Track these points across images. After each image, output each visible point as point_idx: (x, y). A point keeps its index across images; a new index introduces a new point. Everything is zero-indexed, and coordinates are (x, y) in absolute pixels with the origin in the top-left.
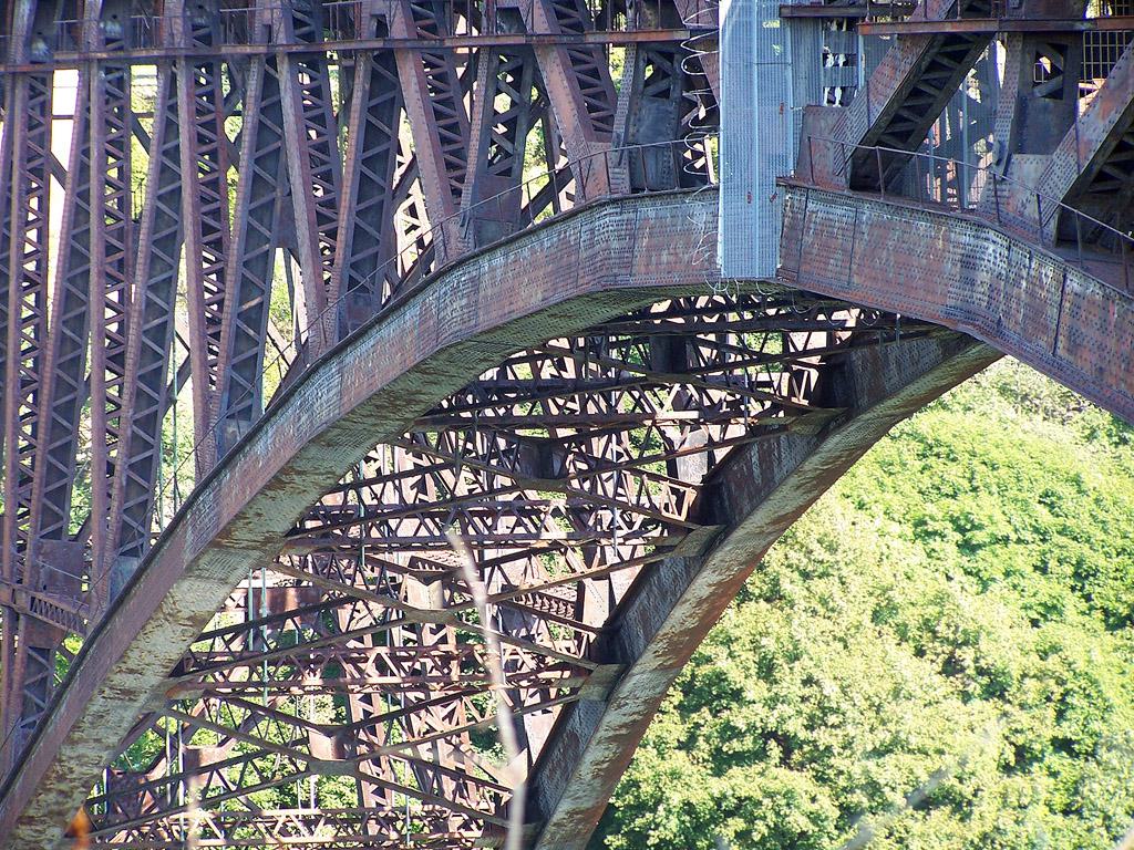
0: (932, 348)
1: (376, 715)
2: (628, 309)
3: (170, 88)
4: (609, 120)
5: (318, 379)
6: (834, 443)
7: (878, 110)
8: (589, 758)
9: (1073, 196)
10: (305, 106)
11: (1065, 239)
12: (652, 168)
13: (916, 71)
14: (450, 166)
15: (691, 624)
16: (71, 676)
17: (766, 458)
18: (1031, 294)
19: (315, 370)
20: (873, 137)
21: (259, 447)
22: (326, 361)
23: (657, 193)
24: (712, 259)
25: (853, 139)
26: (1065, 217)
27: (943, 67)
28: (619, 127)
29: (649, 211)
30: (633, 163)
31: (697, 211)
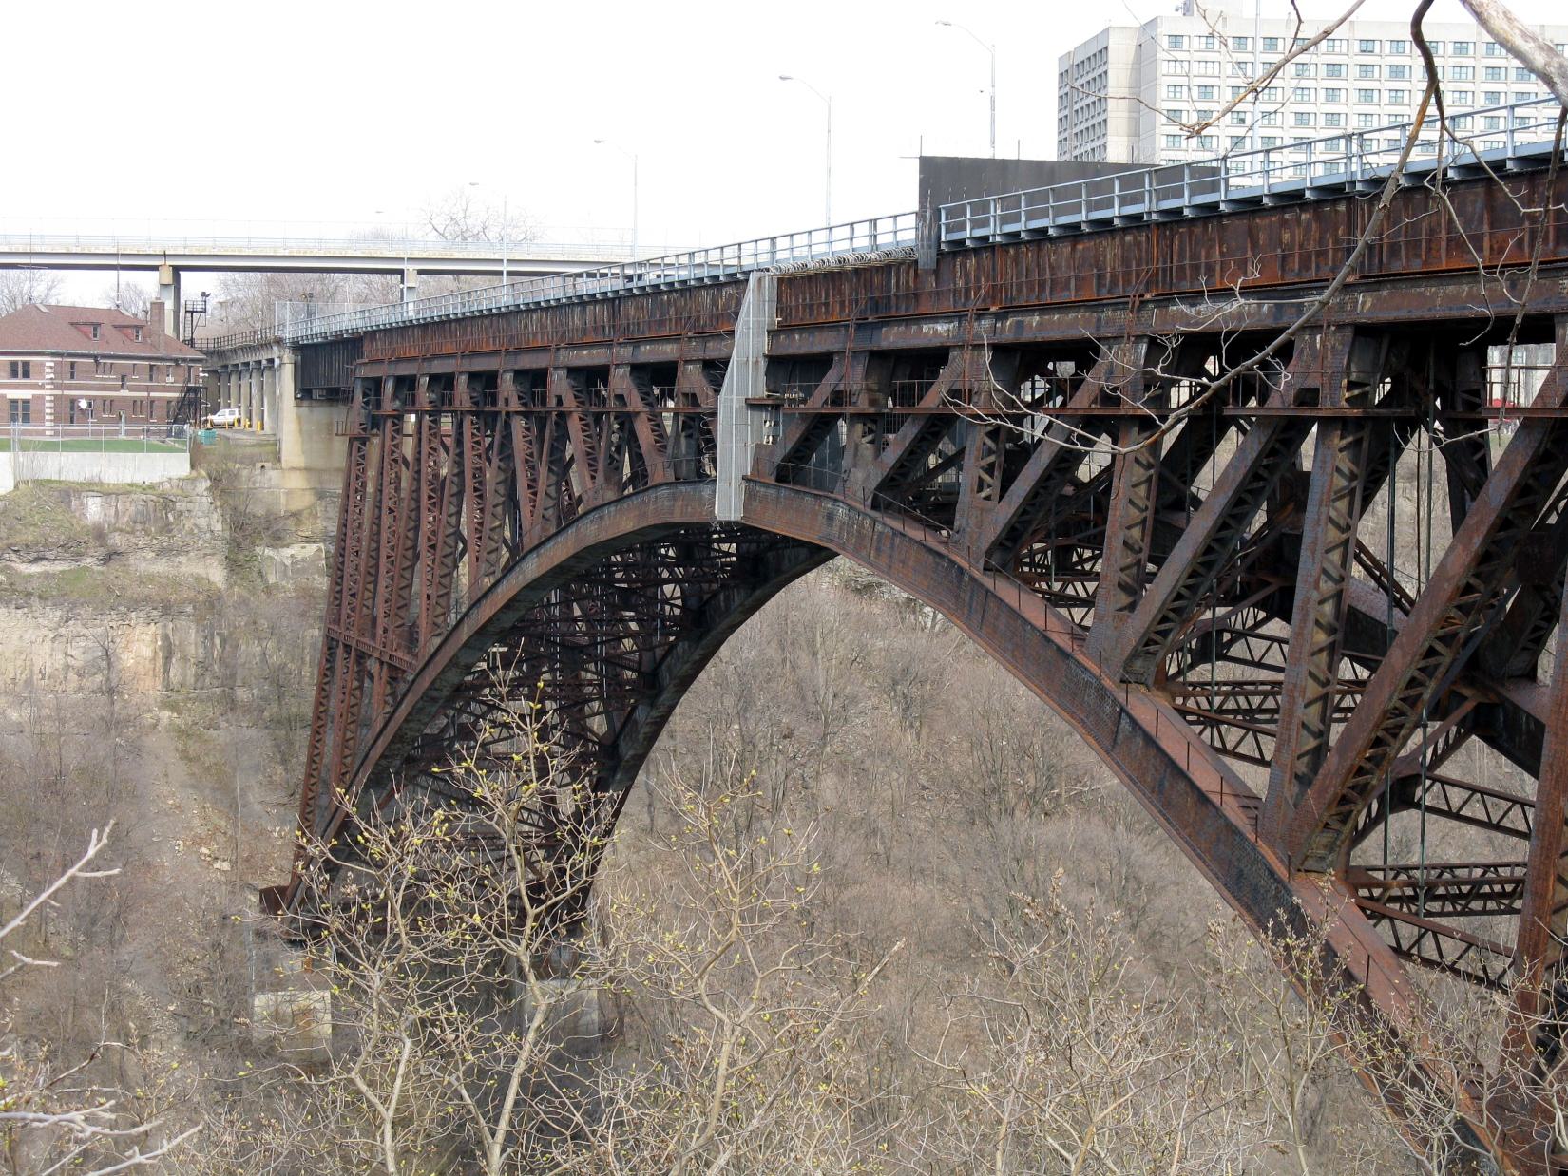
0: (803, 552)
1: (1468, 503)
2: (672, 531)
3: (460, 426)
4: (665, 447)
5: (528, 559)
6: (758, 593)
7: (789, 447)
8: (643, 731)
9: (880, 488)
10: (1373, 670)
11: (875, 507)
12: (684, 470)
13: (807, 429)
14: (590, 465)
15: (690, 672)
16: (408, 691)
17: (727, 599)
18: (859, 532)
19: (526, 555)
20: (787, 458)
21: (499, 589)
22: (531, 551)
23: (687, 482)
24: (713, 512)
25: (778, 459)
26: (875, 498)
27: (1158, 633)
28: (669, 450)
29: (683, 488)
30: (676, 467)
31: (706, 491)
